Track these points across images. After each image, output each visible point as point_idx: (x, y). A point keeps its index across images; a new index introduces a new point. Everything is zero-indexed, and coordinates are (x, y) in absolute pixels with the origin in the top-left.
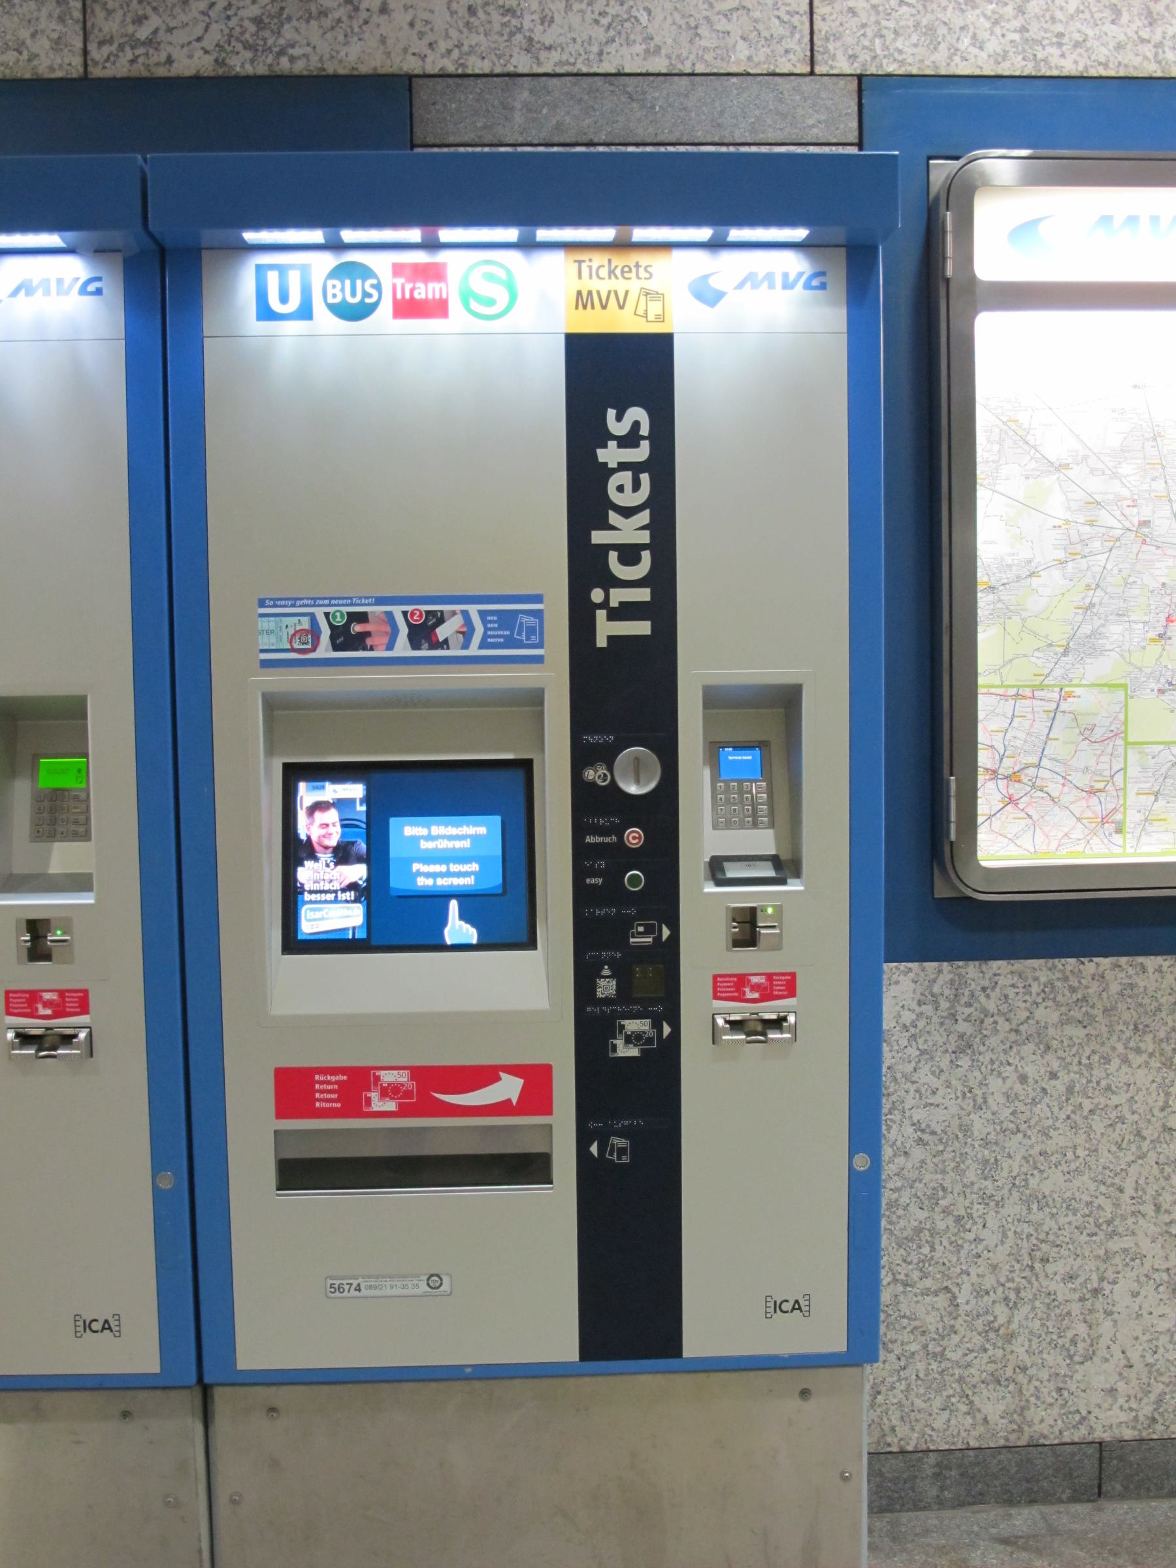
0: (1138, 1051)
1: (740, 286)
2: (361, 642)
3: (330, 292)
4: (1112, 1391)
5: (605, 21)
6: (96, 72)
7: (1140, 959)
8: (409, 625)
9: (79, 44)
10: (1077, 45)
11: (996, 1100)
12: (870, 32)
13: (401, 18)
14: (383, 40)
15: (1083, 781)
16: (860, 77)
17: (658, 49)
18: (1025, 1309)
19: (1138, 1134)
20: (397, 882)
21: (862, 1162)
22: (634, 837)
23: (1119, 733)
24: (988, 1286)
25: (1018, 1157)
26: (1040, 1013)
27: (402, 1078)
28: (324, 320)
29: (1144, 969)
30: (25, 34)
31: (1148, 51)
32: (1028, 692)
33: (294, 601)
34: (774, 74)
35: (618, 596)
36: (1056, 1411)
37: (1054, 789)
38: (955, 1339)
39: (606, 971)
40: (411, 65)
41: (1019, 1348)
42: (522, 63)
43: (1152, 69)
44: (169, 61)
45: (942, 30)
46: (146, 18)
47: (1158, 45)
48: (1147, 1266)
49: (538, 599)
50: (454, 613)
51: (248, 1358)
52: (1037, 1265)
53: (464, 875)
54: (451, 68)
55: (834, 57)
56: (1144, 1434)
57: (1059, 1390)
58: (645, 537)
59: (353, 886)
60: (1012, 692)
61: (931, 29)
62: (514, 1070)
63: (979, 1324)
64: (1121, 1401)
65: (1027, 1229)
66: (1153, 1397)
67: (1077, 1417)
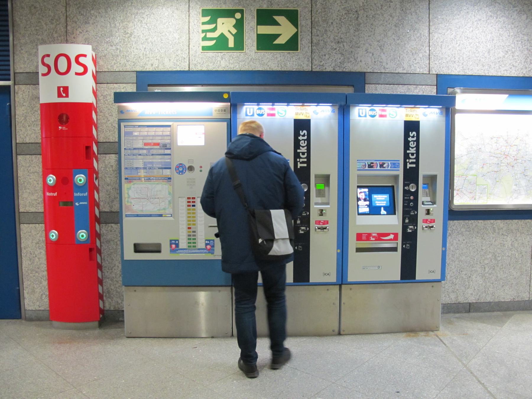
0: (478, 236)
1: (430, 114)
2: (372, 167)
3: (257, 112)
4: (472, 294)
5: (396, 64)
6: (314, 70)
7: (478, 221)
8: (380, 165)
9: (311, 65)
10: (471, 70)
11: (455, 244)
12: (438, 67)
13: (364, 63)
14: (361, 66)
15: (469, 191)
16: (437, 74)
17: (405, 69)
18: (458, 280)
19: (477, 250)
20: (373, 204)
21: (444, 249)
22: (412, 198)
23: (475, 183)
24: (452, 276)
25: (458, 254)
26: (462, 229)
27: (375, 235)
28: (368, 118)
29: (479, 222)
30: (302, 63)
31: (483, 71)
32: (461, 176)
33: (362, 160)
34: (423, 74)
35: (411, 161)
36: (463, 297)
37: (465, 192)
38: (447, 285)
39: (407, 218)
40: (365, 71)
41: (457, 287)
42: (383, 71)
43: (483, 74)
44: (326, 68)
45: (450, 67)
46: (322, 61)
47: (484, 70)
48: (478, 273)
49: (399, 161)
50: (386, 163)
51: (350, 279)
52: (460, 272)
53: (384, 204)
54: (372, 71)
55: (433, 71)
56: (477, 301)
57: (463, 294)
58: (415, 152)
59: (367, 205)
60: (458, 176)
61: (448, 67)
62: (392, 234)
63: (451, 282)
64: (473, 296)
65: (459, 266)
66: (478, 295)
67: (466, 298)
